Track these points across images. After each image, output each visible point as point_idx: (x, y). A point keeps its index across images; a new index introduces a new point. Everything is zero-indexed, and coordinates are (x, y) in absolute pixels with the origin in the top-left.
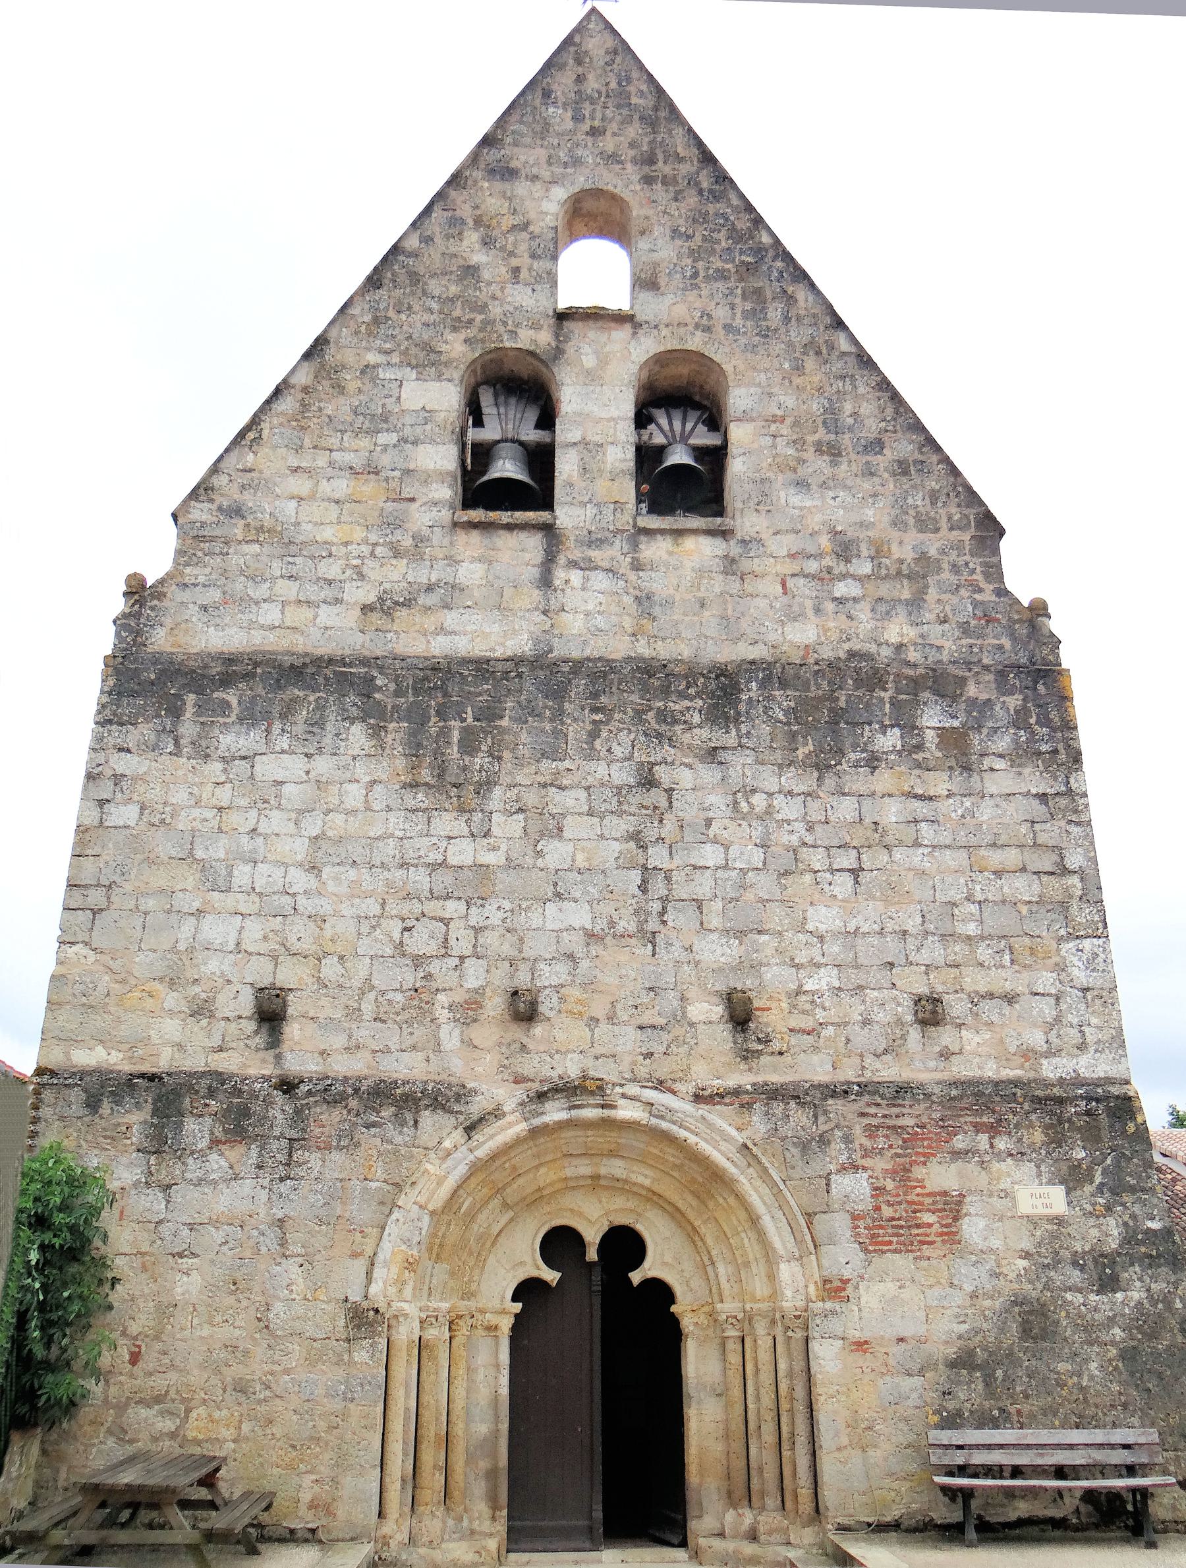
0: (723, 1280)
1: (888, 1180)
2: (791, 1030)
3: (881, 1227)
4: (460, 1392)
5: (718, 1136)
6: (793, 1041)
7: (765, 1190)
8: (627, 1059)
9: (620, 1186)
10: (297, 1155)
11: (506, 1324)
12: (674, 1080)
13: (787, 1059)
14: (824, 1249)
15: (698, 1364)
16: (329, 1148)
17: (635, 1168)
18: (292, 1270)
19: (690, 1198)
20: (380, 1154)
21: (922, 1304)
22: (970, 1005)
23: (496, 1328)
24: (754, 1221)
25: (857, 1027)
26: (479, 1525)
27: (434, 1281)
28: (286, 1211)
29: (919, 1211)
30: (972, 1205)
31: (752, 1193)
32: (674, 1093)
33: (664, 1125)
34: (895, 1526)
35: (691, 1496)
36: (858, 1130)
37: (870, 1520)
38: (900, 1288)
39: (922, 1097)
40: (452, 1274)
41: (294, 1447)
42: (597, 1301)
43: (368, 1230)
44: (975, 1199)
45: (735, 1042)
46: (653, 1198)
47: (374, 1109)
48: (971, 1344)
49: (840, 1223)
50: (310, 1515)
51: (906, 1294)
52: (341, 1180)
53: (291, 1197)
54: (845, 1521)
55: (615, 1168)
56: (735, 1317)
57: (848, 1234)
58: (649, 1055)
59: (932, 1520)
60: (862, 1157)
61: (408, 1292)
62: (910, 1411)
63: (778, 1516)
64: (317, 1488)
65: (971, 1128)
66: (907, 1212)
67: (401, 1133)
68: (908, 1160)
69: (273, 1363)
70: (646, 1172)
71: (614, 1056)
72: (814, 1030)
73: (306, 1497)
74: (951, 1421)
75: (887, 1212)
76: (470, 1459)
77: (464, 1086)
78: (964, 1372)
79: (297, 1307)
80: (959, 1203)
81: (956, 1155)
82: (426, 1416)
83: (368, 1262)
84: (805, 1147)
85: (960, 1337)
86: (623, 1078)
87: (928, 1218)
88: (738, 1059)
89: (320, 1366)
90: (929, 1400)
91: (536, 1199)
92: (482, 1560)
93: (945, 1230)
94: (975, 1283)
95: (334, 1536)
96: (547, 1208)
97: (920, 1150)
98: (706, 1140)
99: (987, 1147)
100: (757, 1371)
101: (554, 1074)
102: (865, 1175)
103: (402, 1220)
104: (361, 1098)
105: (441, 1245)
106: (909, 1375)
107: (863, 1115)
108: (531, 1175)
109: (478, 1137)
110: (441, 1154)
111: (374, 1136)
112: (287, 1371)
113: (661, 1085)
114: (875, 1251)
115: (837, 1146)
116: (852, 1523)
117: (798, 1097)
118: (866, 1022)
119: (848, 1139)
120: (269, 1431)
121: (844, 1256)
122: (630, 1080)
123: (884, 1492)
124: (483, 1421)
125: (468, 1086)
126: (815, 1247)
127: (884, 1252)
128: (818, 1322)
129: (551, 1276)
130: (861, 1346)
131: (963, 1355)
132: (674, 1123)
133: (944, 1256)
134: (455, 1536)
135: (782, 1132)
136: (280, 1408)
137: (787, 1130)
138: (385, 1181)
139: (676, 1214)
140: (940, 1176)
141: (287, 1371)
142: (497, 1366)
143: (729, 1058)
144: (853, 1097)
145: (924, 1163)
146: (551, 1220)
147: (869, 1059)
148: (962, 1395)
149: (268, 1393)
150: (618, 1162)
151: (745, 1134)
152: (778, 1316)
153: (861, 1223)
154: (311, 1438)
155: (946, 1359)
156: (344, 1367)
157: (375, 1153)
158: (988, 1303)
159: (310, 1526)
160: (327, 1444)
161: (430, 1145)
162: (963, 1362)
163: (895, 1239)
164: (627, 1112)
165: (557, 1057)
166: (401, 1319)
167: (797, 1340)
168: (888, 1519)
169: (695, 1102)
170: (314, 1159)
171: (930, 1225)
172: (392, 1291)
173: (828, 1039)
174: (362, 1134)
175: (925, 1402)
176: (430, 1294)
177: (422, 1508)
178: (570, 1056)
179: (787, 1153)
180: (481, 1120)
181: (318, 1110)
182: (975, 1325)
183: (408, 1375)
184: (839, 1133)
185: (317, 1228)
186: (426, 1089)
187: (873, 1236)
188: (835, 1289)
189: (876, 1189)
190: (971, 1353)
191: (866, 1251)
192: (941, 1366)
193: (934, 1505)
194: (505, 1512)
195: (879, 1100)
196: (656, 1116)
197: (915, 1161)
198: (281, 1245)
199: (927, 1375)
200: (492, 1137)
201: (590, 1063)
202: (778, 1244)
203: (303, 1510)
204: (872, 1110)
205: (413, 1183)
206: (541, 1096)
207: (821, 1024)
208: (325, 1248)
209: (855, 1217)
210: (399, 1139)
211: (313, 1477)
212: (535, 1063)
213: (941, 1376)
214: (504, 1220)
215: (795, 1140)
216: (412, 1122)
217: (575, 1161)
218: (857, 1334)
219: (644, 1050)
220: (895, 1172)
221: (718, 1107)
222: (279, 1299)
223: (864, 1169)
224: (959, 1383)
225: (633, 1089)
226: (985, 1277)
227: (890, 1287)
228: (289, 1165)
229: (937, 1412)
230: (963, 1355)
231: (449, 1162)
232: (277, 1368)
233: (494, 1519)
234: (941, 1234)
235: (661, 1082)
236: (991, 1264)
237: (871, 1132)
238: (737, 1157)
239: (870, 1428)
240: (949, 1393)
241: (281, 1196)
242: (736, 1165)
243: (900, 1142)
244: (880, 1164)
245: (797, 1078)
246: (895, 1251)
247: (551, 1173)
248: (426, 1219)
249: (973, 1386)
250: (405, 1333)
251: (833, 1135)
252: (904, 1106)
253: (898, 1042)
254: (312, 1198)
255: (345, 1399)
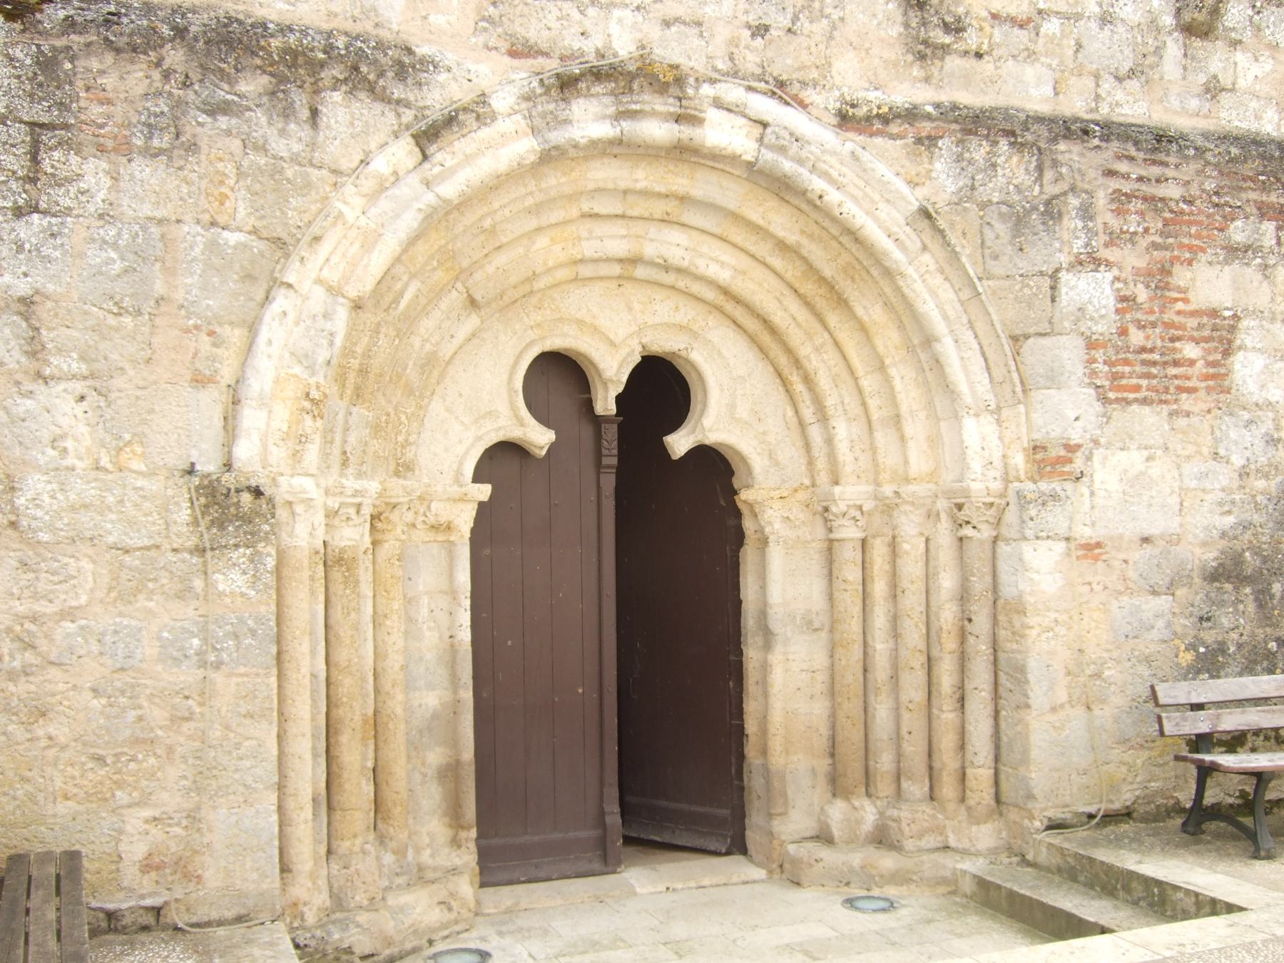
0: (842, 448)
1: (1140, 286)
2: (995, 16)
3: (1126, 362)
4: (395, 640)
5: (876, 190)
6: (998, 35)
7: (947, 294)
8: (723, 33)
9: (673, 278)
10: (52, 160)
11: (465, 520)
12: (804, 84)
13: (987, 66)
14: (1036, 396)
15: (782, 582)
16: (124, 149)
17: (705, 249)
18: (62, 410)
19: (795, 307)
20: (240, 174)
21: (1176, 484)
22: (1250, 12)
23: (449, 528)
24: (923, 343)
25: (1093, 25)
26: (432, 856)
27: (352, 439)
28: (39, 279)
29: (1179, 339)
30: (1249, 333)
31: (927, 297)
32: (803, 105)
33: (788, 166)
34: (1127, 814)
35: (755, 782)
36: (1101, 200)
37: (1091, 809)
38: (1148, 460)
39: (1192, 152)
40: (377, 429)
41: (100, 760)
42: (609, 482)
43: (226, 331)
44: (1252, 323)
45: (907, 26)
46: (729, 304)
47: (223, 74)
48: (1238, 546)
49: (1068, 352)
50: (148, 882)
51: (1155, 470)
52: (160, 222)
53: (46, 251)
54: (1057, 814)
55: (671, 245)
56: (860, 508)
57: (1080, 370)
58: (760, 30)
59: (1178, 802)
60: (1106, 245)
61: (312, 454)
62: (1153, 648)
63: (927, 809)
64: (156, 832)
65: (1255, 211)
66: (1162, 339)
67: (283, 133)
68: (1168, 254)
69: (36, 597)
70: (725, 258)
71: (699, 24)
72: (1029, 20)
73: (135, 850)
74: (1210, 662)
75: (1136, 338)
76: (414, 748)
77: (409, 51)
78: (1228, 587)
79: (79, 485)
80: (1232, 329)
81: (1235, 252)
82: (346, 684)
83: (226, 398)
84: (1019, 222)
85: (1223, 535)
86: (715, 70)
87: (1190, 351)
88: (910, 58)
89: (142, 602)
90: (1179, 630)
91: (520, 295)
92: (453, 915)
93: (1211, 371)
94: (1248, 454)
95: (201, 914)
96: (536, 317)
97: (1186, 241)
98: (854, 198)
99: (1274, 242)
100: (894, 592)
101: (589, 47)
102: (1109, 276)
103: (292, 316)
104: (191, 49)
105: (363, 372)
106: (1155, 593)
107: (1110, 173)
108: (521, 250)
109: (442, 156)
110: (368, 185)
111: (228, 133)
112: (69, 614)
113: (780, 90)
114: (1117, 400)
115: (1071, 222)
116: (1068, 816)
117: (1013, 134)
118: (1106, 20)
119: (1087, 213)
120: (41, 732)
121: (1069, 409)
122: (727, 74)
123: (1111, 768)
124: (430, 687)
125: (417, 50)
126: (1024, 391)
127: (1129, 402)
128: (1033, 513)
129: (540, 437)
130: (1092, 549)
131: (1228, 562)
132: (800, 162)
133: (1209, 411)
134: (399, 880)
135: (983, 193)
136: (61, 687)
137: (991, 191)
138: (254, 232)
139: (764, 336)
140: (1210, 284)
141: (69, 614)
142: (453, 593)
143: (895, 53)
144: (1096, 142)
145: (1190, 263)
146: (543, 338)
147: (1107, 84)
148: (1226, 622)
149: (29, 656)
150: (677, 236)
151: (921, 192)
152: (942, 504)
153: (1099, 355)
154: (137, 741)
155: (1203, 569)
156: (195, 603)
157: (230, 169)
158: (1261, 484)
159: (149, 902)
160: (170, 750)
161: (345, 165)
162: (1227, 572)
163: (1144, 383)
164: (722, 132)
165: (592, 12)
166: (299, 509)
167: (981, 542)
168: (1117, 806)
169: (840, 126)
170: (94, 174)
171: (1192, 363)
172: (279, 455)
173: (1051, 39)
174: (200, 125)
175: (1175, 633)
176: (345, 464)
177: (347, 844)
178: (617, 13)
179: (987, 231)
180: (450, 120)
181: (95, 64)
182: (1243, 516)
183: (313, 615)
184: (1074, 202)
185: (112, 321)
186: (332, 47)
187: (1115, 377)
188: (1054, 462)
189: (1124, 299)
190: (1238, 560)
191: (1104, 400)
192: (1197, 580)
193: (1181, 782)
194: (473, 833)
195: (1133, 152)
196: (770, 147)
197: (1178, 258)
198: (33, 354)
199: (1178, 593)
200: (468, 159)
201: (654, 32)
202: (963, 387)
203: (130, 874)
204: (1123, 167)
205: (317, 239)
206: (566, 85)
207: (1040, 12)
208: (134, 362)
209: (1091, 345)
210: (279, 146)
211: (147, 813)
212: (551, 19)
213: (1194, 594)
214: (463, 331)
215: (1004, 209)
216: (305, 114)
217: (600, 228)
218: (1087, 532)
219: (752, 19)
220: (1150, 274)
221: (878, 140)
222: (38, 468)
223: (1109, 265)
224: (1222, 604)
225: (733, 92)
226: (1259, 444)
227: (1133, 459)
228: (34, 181)
229: (1192, 647)
230: (1228, 562)
231: (384, 204)
232: (42, 607)
233: (455, 843)
234: (1207, 377)
235: (781, 84)
236: (1267, 426)
237: (1120, 201)
238: (905, 233)
239: (1097, 675)
240: (1208, 619)
241: (20, 248)
242: (903, 248)
243: (1160, 225)
244: (1132, 259)
245: (1001, 101)
246: (1145, 401)
247: (557, 248)
248: (342, 315)
249: (1241, 607)
250: (304, 534)
251: (1066, 203)
252: (1166, 164)
253: (1151, 60)
254: (95, 256)
255: (203, 664)
